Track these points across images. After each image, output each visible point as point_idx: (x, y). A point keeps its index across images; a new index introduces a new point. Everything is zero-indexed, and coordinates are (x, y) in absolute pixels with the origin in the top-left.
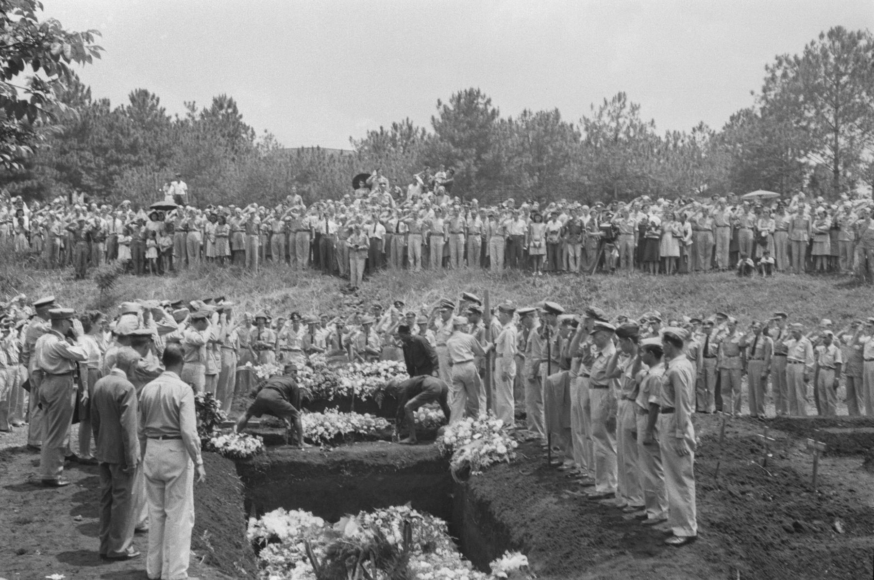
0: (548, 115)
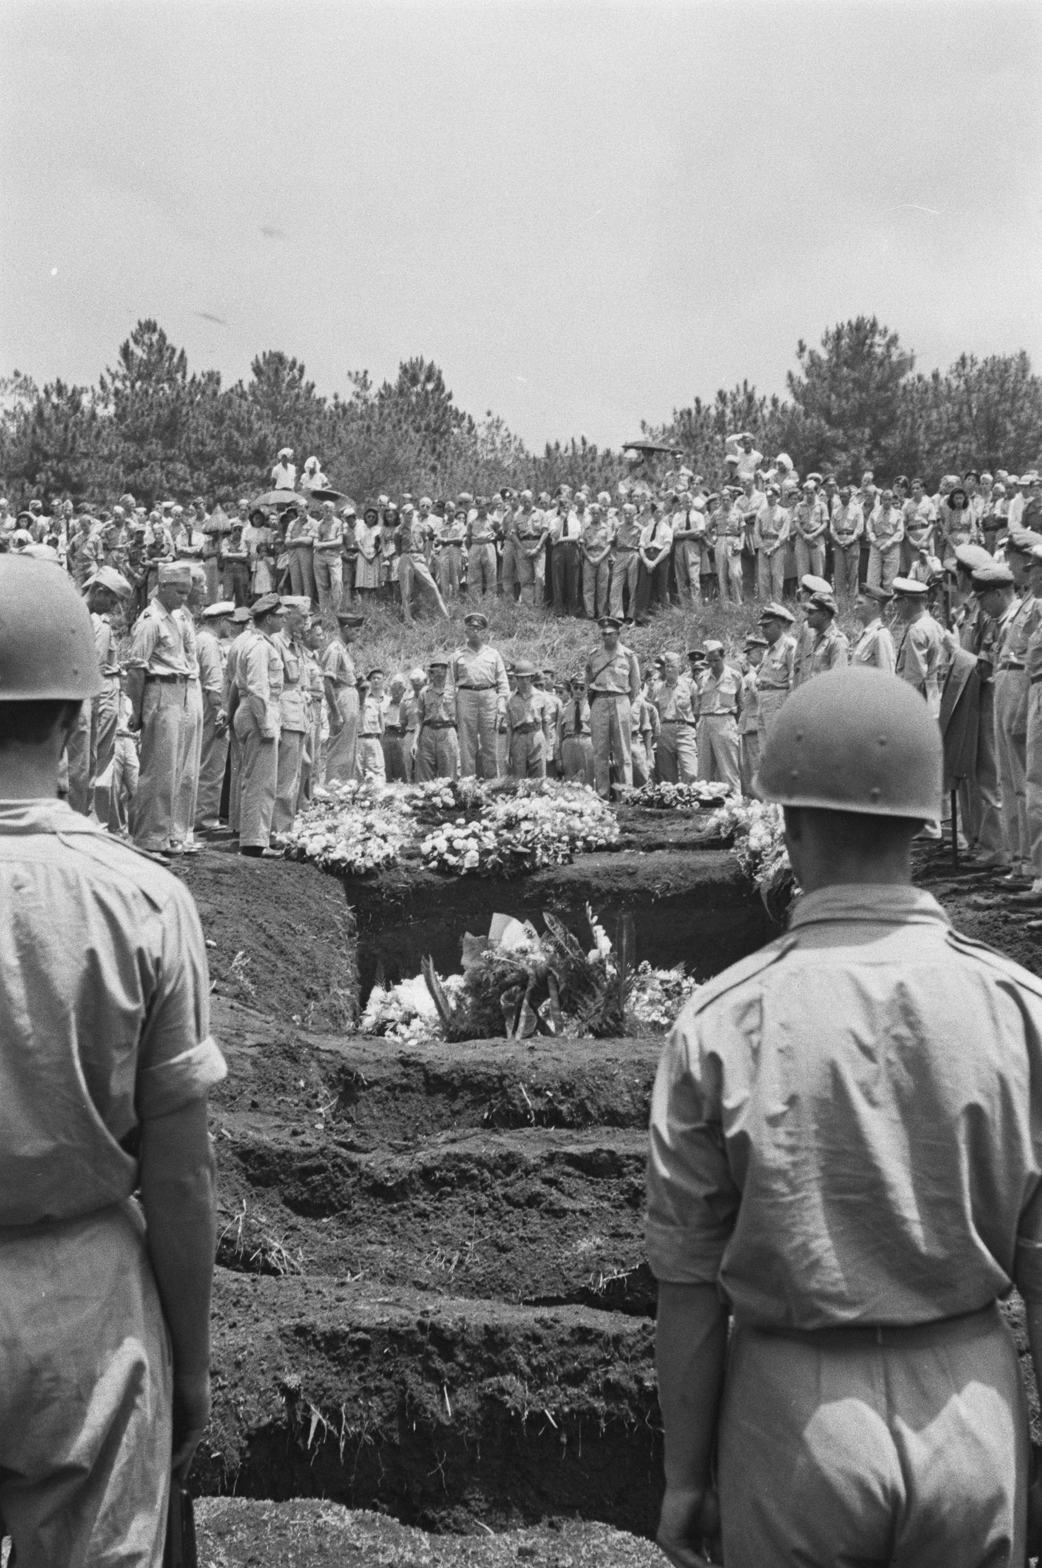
0: (1007, 364)
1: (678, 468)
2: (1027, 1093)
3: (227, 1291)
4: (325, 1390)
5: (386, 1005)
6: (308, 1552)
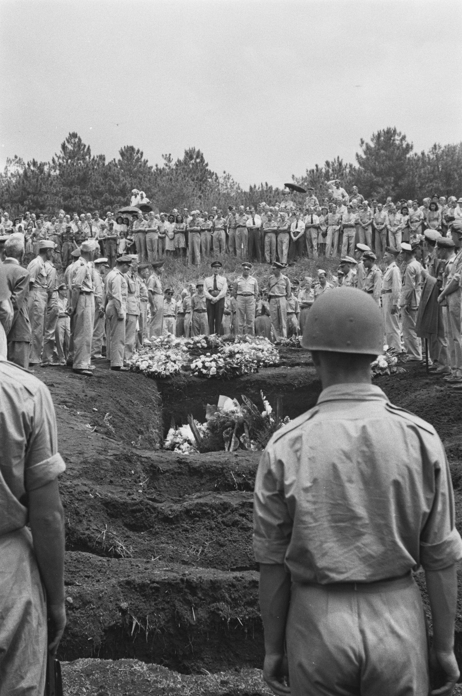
0: (455, 148)
1: (311, 196)
2: (421, 475)
3: (96, 565)
4: (139, 609)
5: (175, 436)
6: (127, 683)
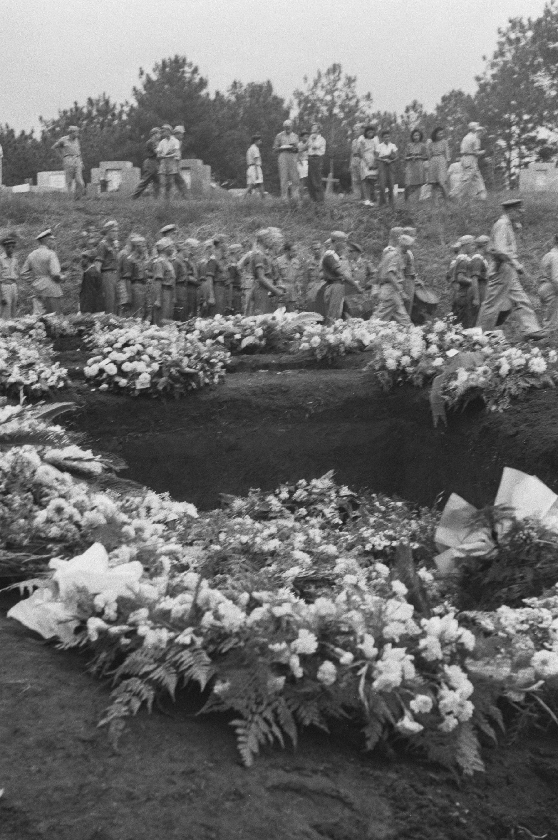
0: (261, 87)
